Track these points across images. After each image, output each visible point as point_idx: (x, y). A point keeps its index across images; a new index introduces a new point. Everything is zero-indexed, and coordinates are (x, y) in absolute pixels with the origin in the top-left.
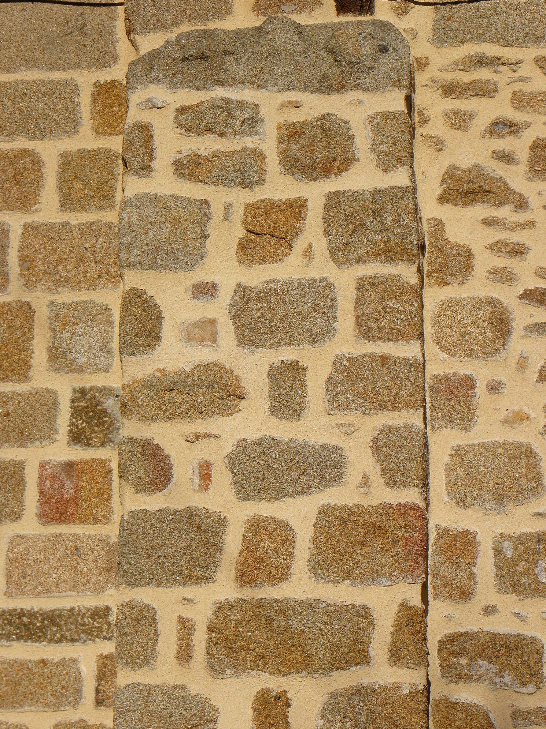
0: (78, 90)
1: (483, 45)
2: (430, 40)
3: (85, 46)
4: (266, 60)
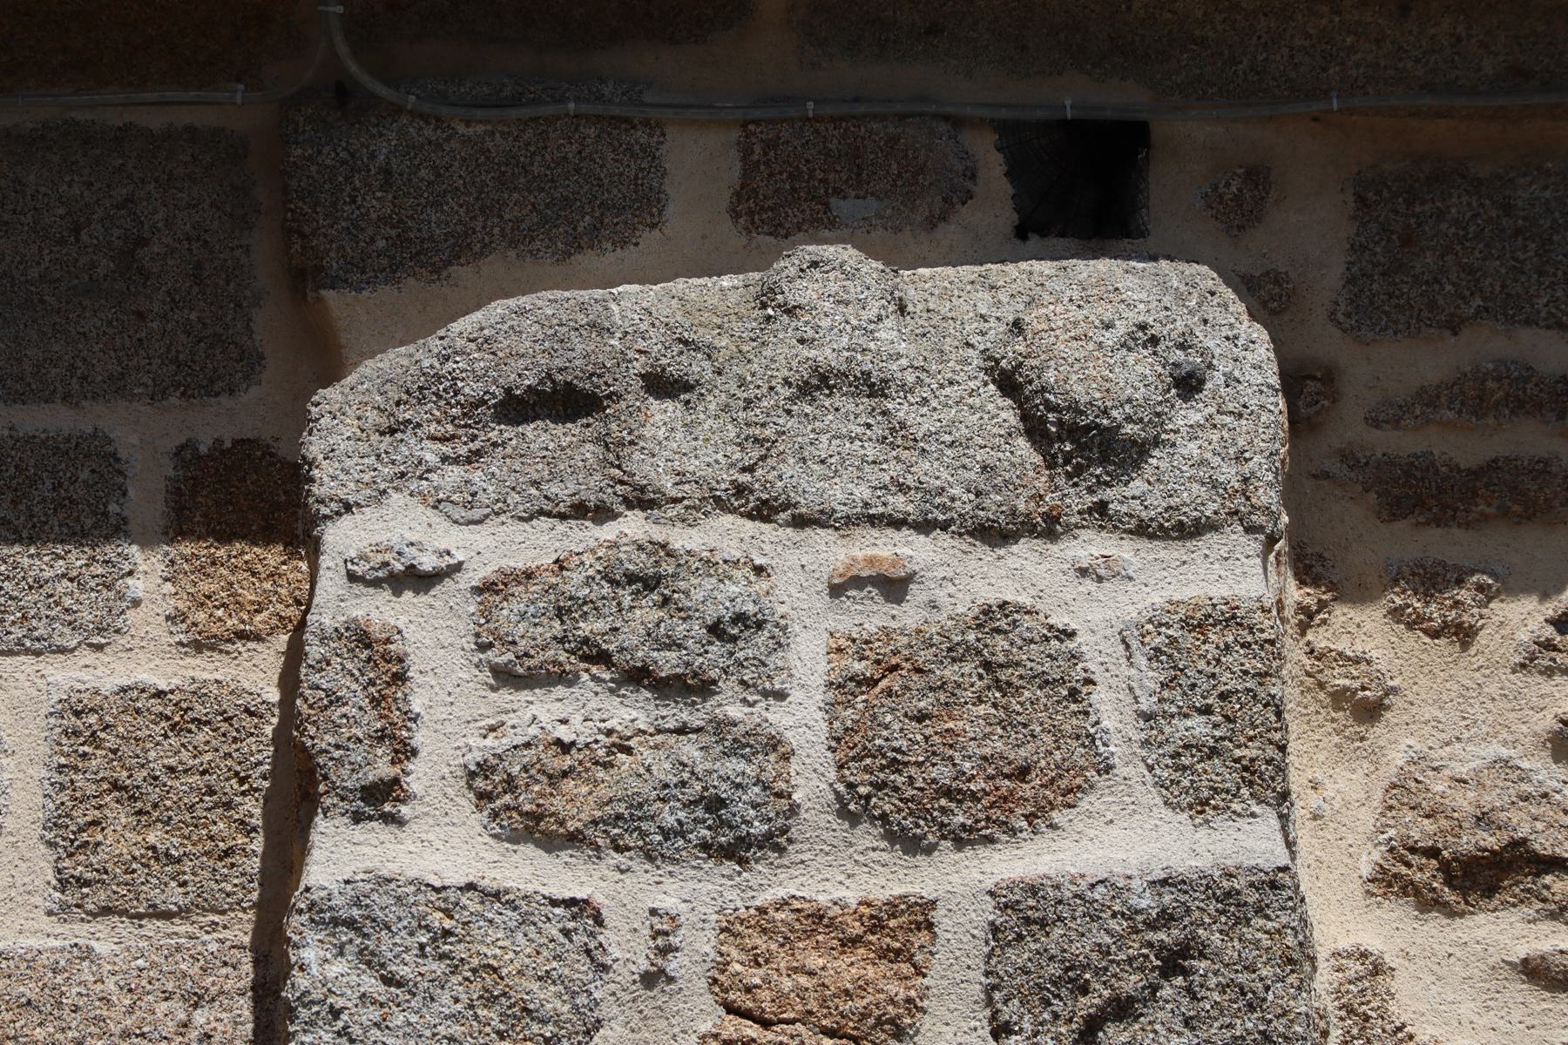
0: (120, 472)
1: (1526, 335)
2: (1340, 317)
3: (140, 315)
4: (789, 412)
